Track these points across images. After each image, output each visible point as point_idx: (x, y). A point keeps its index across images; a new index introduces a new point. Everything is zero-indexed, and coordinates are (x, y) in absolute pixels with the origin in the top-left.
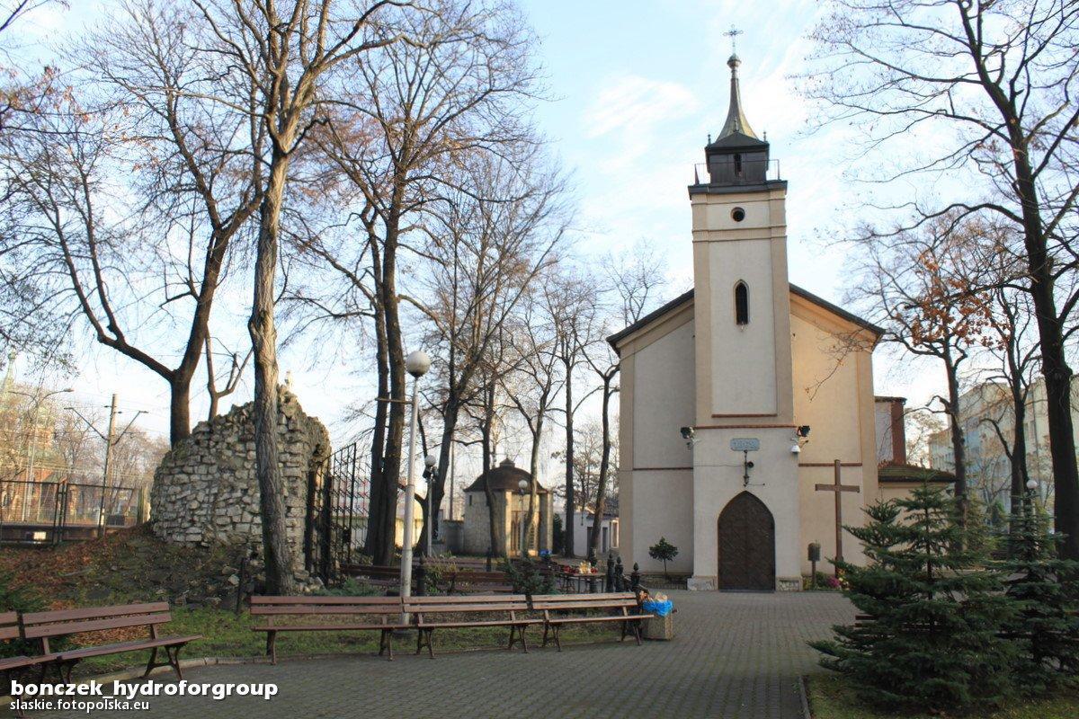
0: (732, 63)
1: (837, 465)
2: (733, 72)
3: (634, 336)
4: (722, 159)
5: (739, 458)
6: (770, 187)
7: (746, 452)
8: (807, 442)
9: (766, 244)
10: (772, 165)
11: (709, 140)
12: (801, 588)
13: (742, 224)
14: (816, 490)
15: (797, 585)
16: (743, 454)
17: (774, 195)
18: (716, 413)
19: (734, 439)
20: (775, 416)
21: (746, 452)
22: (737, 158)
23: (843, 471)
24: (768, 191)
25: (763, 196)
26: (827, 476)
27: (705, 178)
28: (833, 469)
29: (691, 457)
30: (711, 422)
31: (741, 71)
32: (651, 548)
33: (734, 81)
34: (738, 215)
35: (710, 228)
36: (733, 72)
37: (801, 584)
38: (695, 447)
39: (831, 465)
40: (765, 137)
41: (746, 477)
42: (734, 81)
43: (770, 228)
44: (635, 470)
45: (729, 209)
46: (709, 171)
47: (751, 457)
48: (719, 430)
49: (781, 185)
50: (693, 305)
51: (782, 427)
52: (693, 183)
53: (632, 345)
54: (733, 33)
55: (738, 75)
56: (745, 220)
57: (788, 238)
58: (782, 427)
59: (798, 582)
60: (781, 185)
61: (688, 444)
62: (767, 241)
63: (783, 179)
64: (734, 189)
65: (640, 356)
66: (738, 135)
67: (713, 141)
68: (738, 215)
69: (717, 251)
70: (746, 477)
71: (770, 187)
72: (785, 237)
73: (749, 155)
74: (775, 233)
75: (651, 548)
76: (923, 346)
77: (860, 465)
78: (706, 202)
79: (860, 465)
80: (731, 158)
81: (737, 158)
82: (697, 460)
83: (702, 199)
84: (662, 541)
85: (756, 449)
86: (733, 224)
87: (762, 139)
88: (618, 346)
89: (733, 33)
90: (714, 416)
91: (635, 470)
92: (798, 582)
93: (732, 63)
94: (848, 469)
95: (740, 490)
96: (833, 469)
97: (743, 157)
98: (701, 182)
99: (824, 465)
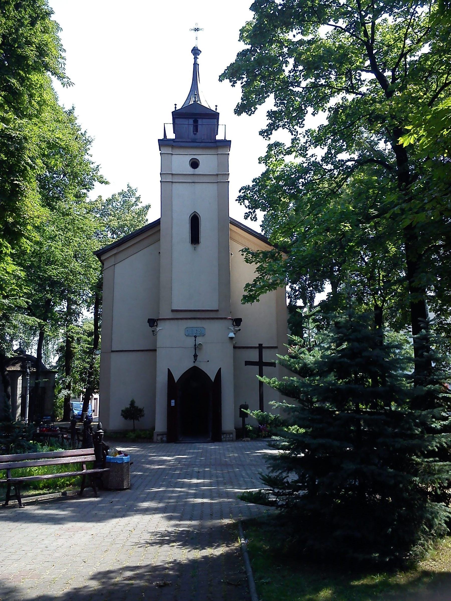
0: (196, 52)
1: (261, 347)
2: (196, 58)
3: (114, 251)
4: (185, 121)
5: (190, 342)
6: (218, 144)
7: (195, 337)
8: (240, 330)
9: (215, 186)
10: (221, 129)
11: (176, 108)
12: (235, 438)
13: (198, 171)
14: (245, 365)
15: (231, 436)
16: (194, 338)
17: (220, 151)
18: (174, 308)
19: (187, 328)
20: (217, 311)
21: (195, 337)
22: (196, 122)
23: (265, 352)
24: (217, 147)
25: (213, 152)
26: (254, 356)
27: (171, 135)
28: (257, 360)
29: (155, 342)
30: (171, 316)
31: (200, 58)
32: (122, 411)
33: (196, 65)
34: (195, 164)
35: (174, 172)
36: (196, 58)
37: (235, 434)
38: (158, 334)
39: (255, 348)
40: (216, 109)
41: (195, 356)
42: (196, 65)
43: (217, 175)
44: (112, 351)
45: (186, 160)
46: (174, 133)
47: (200, 340)
48: (176, 321)
49: (226, 144)
50: (160, 230)
51: (221, 319)
52: (162, 137)
53: (113, 259)
54: (197, 30)
55: (199, 61)
56: (199, 167)
57: (230, 184)
58: (221, 319)
59: (232, 433)
60: (226, 144)
61: (153, 331)
62: (216, 156)
63: (227, 139)
64: (192, 144)
65: (119, 268)
66: (197, 106)
67: (179, 107)
68: (195, 164)
69: (178, 189)
70: (195, 356)
71: (218, 144)
72: (229, 154)
73: (204, 120)
74: (220, 179)
75: (122, 411)
76: (328, 169)
77: (276, 347)
78: (171, 152)
79: (276, 347)
80: (191, 121)
81: (196, 122)
82: (159, 344)
83: (168, 150)
84: (132, 403)
85: (204, 335)
86: (190, 170)
87: (213, 108)
88: (103, 258)
89: (197, 30)
90: (173, 311)
91: (112, 351)
92: (232, 433)
93: (196, 52)
94: (268, 350)
95: (191, 365)
96: (257, 350)
97: (200, 122)
98: (168, 137)
99: (251, 348)
